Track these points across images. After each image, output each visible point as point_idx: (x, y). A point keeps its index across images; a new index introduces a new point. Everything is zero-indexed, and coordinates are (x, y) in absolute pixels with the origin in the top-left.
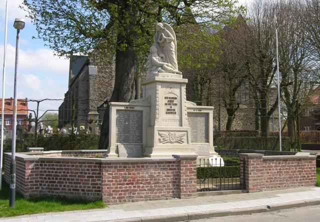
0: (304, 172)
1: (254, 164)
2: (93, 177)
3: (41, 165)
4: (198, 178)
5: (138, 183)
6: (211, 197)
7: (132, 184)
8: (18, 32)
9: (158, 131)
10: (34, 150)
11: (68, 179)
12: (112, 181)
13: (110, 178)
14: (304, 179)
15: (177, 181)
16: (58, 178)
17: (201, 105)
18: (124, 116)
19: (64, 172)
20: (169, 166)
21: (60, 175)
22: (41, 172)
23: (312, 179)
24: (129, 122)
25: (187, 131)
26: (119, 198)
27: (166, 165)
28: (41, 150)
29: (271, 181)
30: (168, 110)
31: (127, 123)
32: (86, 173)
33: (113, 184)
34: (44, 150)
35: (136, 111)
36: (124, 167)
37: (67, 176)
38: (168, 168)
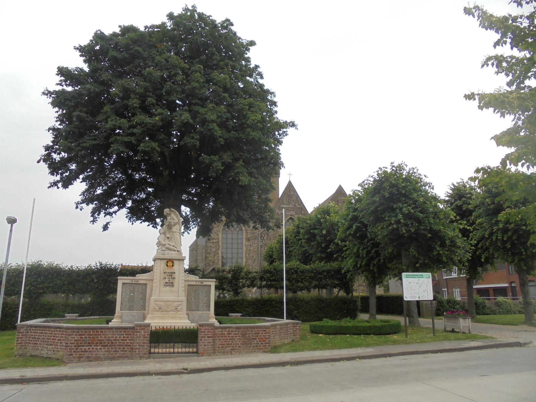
1: (205, 332)
2: (60, 340)
3: (30, 330)
4: (150, 343)
5: (96, 346)
7: (91, 346)
8: (12, 226)
10: (70, 316)
11: (46, 341)
12: (74, 343)
14: (257, 346)
20: (125, 332)
24: (134, 293)
26: (78, 358)
28: (76, 316)
29: (222, 347)
30: (166, 283)
32: (57, 337)
33: (75, 346)
34: (79, 316)
35: (140, 284)
37: (44, 339)
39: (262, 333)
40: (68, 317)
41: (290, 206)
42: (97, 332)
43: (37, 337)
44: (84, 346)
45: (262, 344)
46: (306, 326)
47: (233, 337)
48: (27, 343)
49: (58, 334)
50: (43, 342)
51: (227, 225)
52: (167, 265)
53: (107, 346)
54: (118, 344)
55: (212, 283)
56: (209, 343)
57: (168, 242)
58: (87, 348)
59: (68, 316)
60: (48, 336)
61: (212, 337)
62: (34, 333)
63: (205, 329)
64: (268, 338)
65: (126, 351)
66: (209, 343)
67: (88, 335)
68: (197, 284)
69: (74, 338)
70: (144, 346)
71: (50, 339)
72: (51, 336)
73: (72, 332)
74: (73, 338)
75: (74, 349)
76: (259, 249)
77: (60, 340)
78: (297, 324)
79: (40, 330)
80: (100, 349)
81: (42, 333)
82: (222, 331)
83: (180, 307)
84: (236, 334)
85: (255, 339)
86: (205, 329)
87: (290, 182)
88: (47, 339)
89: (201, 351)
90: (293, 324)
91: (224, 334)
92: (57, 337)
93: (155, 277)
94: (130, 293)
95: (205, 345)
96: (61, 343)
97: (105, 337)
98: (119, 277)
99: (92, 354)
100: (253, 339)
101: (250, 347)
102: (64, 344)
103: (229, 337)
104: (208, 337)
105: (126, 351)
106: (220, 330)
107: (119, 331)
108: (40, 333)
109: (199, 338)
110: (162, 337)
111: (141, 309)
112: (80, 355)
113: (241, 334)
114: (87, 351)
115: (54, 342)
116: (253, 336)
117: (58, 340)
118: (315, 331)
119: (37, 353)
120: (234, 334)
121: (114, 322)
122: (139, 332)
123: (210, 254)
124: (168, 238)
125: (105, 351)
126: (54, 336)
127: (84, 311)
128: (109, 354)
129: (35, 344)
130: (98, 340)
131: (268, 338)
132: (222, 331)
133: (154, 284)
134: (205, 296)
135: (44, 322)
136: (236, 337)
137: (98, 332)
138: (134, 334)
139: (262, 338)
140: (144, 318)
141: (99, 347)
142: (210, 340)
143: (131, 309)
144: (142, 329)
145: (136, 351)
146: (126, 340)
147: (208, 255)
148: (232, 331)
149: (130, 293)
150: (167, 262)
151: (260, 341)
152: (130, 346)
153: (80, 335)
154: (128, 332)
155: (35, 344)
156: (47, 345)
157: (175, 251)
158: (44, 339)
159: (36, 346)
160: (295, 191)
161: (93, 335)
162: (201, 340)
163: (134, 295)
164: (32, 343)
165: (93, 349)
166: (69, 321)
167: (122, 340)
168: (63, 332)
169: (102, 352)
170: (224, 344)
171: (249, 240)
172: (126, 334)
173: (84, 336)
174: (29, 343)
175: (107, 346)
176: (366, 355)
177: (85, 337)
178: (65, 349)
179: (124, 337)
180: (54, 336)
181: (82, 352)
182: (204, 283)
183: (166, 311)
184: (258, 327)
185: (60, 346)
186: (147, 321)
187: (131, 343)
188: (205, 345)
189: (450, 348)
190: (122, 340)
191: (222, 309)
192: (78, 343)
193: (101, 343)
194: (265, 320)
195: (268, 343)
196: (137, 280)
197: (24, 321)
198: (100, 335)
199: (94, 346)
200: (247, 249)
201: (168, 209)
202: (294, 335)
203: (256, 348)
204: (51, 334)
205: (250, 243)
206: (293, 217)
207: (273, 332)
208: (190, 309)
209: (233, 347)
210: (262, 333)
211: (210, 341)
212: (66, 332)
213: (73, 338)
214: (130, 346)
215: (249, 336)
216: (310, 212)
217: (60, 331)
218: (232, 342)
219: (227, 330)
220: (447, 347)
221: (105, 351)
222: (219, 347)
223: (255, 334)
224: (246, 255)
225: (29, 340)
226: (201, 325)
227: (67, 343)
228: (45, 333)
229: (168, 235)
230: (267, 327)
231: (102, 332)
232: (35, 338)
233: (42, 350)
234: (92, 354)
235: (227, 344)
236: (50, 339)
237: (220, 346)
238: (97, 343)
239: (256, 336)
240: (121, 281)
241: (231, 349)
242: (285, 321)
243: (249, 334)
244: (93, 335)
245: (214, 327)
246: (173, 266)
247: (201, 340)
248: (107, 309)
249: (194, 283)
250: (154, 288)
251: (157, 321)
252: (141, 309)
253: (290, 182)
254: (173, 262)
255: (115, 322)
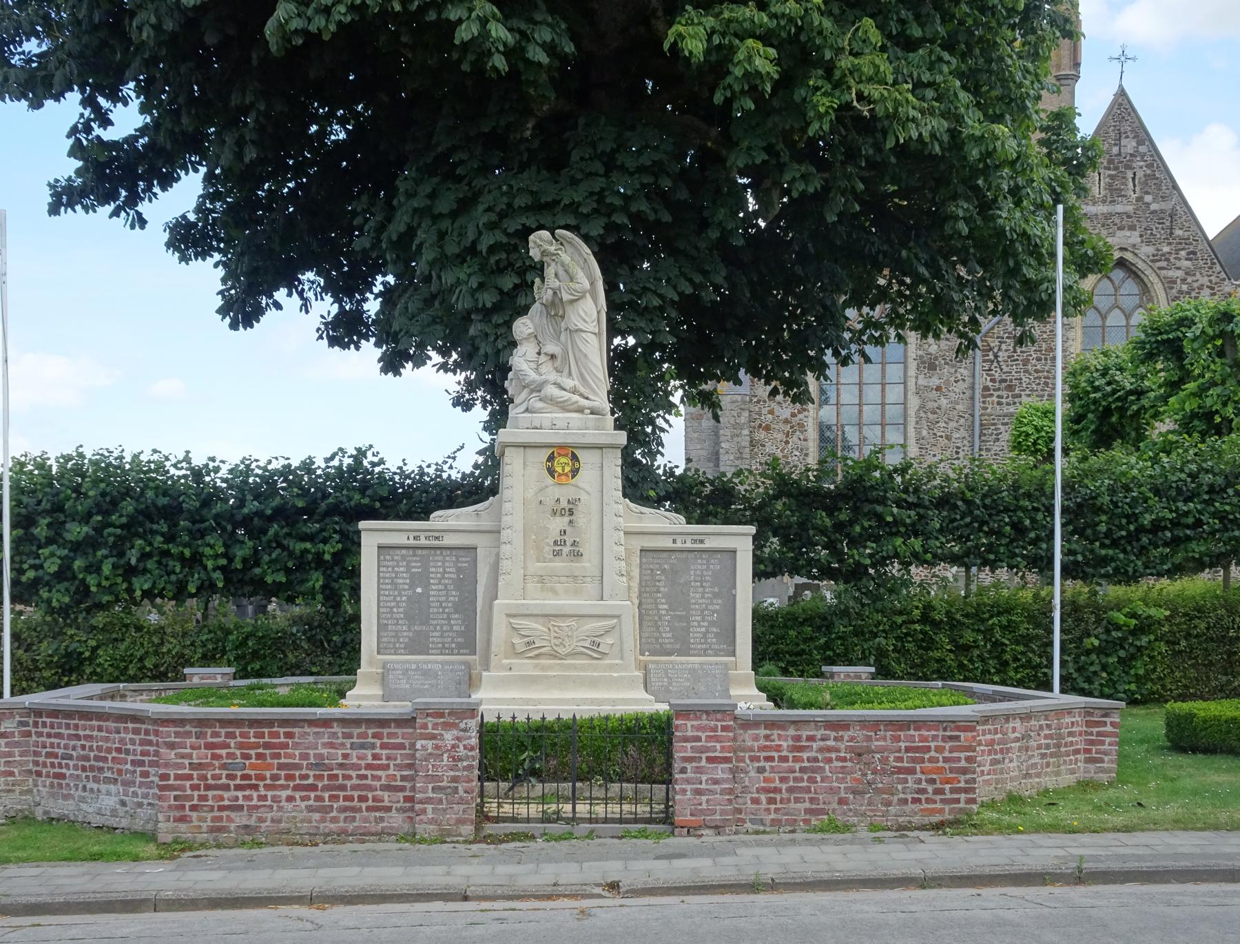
0: (919, 775)
1: (698, 739)
2: (142, 763)
4: (486, 774)
6: (895, 872)
7: (256, 787)
8: (1121, 86)
9: (509, 616)
11: (92, 769)
12: (190, 777)
13: (182, 766)
15: (408, 785)
16: (778, 797)
17: (1053, 506)
18: (408, 567)
19: (83, 747)
21: (74, 753)
22: (36, 744)
23: (958, 801)
24: (427, 586)
25: (618, 617)
27: (370, 732)
29: (771, 801)
31: (419, 590)
32: (127, 752)
33: (195, 787)
36: (228, 735)
38: (378, 742)
39: (939, 749)
40: (196, 680)
41: (1119, 208)
42: (272, 735)
43: (61, 751)
44: (226, 788)
45: (938, 792)
46: (1152, 721)
47: (816, 760)
48: (30, 772)
49: (133, 742)
50: (84, 769)
51: (164, 189)
52: (551, 472)
53: (313, 788)
54: (355, 781)
55: (739, 540)
56: (716, 782)
57: (553, 376)
58: (240, 794)
59: (197, 675)
60: (99, 749)
61: (727, 760)
62: (49, 735)
63: (699, 728)
64: (964, 771)
65: (389, 809)
66: (716, 782)
67: (241, 746)
68: (679, 545)
69: (190, 756)
70: (456, 790)
71: (105, 759)
72: (109, 750)
73: (177, 734)
74: (183, 756)
75: (191, 798)
76: (978, 405)
77: (142, 763)
78: (1107, 712)
79: (68, 726)
80: (290, 799)
81: (78, 737)
82: (767, 737)
83: (609, 640)
84: (829, 749)
85: (912, 771)
86: (699, 728)
87: (1122, 93)
88: (97, 758)
89: (683, 814)
90: (1088, 711)
91: (778, 748)
92: (127, 752)
93: (506, 520)
94: (412, 586)
95: (698, 792)
96: (145, 774)
97: (305, 757)
98: (363, 524)
99: (261, 820)
100: (900, 770)
101: (889, 804)
102: (156, 779)
103: (796, 759)
104: (709, 760)
105: (389, 809)
106: (763, 732)
107: (356, 731)
108: (70, 737)
109: (677, 765)
110: (515, 754)
111: (460, 646)
112: (214, 819)
113: (850, 749)
114: (241, 808)
115: (120, 772)
116: (900, 759)
117: (133, 763)
118: (1187, 740)
119: (59, 807)
120: (821, 750)
121: (358, 697)
122: (433, 737)
123: (767, 428)
124: (553, 357)
125: (310, 809)
126: (119, 750)
127: (258, 658)
128: (323, 820)
129: (57, 776)
130: (281, 767)
131: (964, 771)
132: (767, 737)
133: (505, 549)
134: (716, 595)
135: (102, 697)
136: (830, 760)
137: (277, 735)
138: (413, 745)
139: (940, 770)
140: (472, 682)
141: (284, 794)
142: (721, 771)
143: (418, 646)
144: (448, 726)
145: (424, 811)
146: (387, 767)
147: (761, 435)
148: (811, 738)
149: (412, 586)
150: (551, 458)
151: (933, 781)
152: (402, 789)
153: (209, 746)
154: (390, 735)
155: (57, 776)
156: (96, 780)
157: (580, 410)
158: (87, 758)
159: (60, 785)
160: (1142, 135)
161: (257, 746)
162: (683, 770)
163: (426, 594)
164: (48, 776)
165: (262, 798)
166: (205, 695)
167: (368, 767)
168: (147, 732)
169: (296, 810)
170: (777, 790)
171: (932, 367)
172: (383, 746)
173: (223, 752)
174: (39, 774)
175: (313, 788)
176: (987, 871)
177: (229, 755)
178: (160, 798)
179: (375, 757)
180: (119, 750)
181: (221, 808)
182: (710, 543)
183: (555, 655)
184: (919, 724)
185: (141, 785)
186: (476, 696)
187: (403, 778)
188: (698, 792)
189: (89, 918)
190: (368, 767)
191: (785, 647)
192: (204, 778)
193: (290, 777)
194: (971, 694)
195: (966, 791)
196: (439, 533)
197: (23, 691)
198: (286, 746)
199: (267, 787)
200: (922, 407)
201: (545, 234)
202: (1088, 761)
203: (916, 807)
204: (107, 739)
205: (935, 381)
206: (1128, 256)
207: (991, 743)
208: (651, 645)
209: (812, 800)
210: (939, 749)
211: (720, 775)
212: (157, 733)
213: (183, 756)
214: (402, 789)
215: (884, 761)
216: (1211, 233)
217: (136, 731)
218: (812, 780)
219: (791, 732)
220: (770, 871)
221: (310, 809)
222: (756, 801)
223: (908, 750)
224: (918, 431)
225: (36, 763)
226: (685, 712)
227: (164, 777)
228: (87, 737)
229: (551, 348)
230: (968, 725)
231: (289, 735)
232: (56, 756)
233: (83, 800)
234: (261, 820)
235: (790, 790)
236: (105, 759)
237: (763, 797)
238: (275, 777)
239: (913, 760)
240: (374, 536)
241: (807, 811)
242: (1056, 698)
243: (881, 750)
244: (257, 746)
245: (735, 718)
246: (575, 472)
247: (683, 770)
248: (332, 646)
249: (667, 543)
250: (505, 565)
251: (511, 694)
252: (460, 646)
253: (1122, 93)
254: (575, 458)
255: (364, 696)
